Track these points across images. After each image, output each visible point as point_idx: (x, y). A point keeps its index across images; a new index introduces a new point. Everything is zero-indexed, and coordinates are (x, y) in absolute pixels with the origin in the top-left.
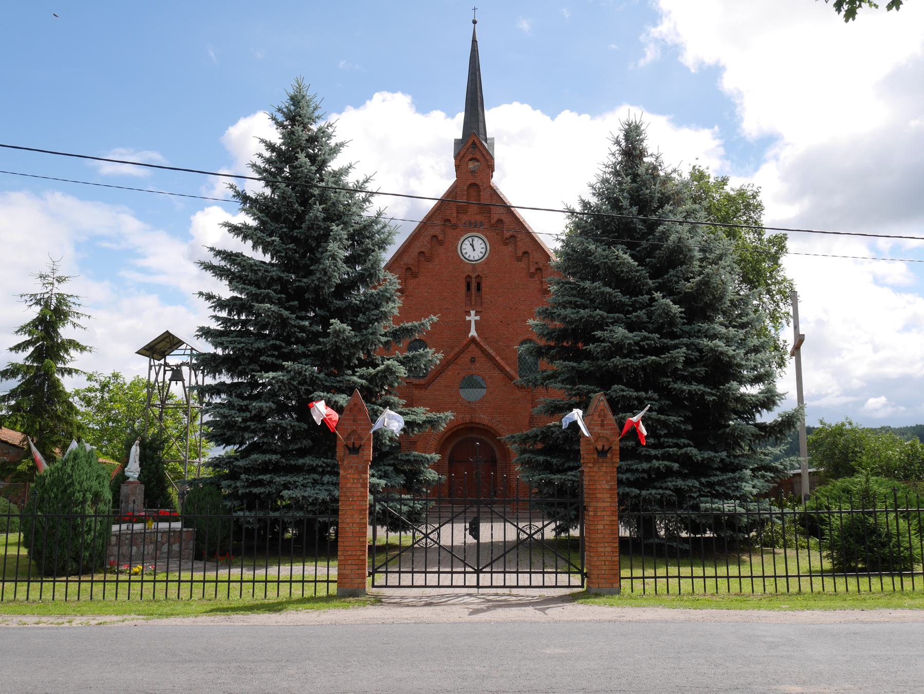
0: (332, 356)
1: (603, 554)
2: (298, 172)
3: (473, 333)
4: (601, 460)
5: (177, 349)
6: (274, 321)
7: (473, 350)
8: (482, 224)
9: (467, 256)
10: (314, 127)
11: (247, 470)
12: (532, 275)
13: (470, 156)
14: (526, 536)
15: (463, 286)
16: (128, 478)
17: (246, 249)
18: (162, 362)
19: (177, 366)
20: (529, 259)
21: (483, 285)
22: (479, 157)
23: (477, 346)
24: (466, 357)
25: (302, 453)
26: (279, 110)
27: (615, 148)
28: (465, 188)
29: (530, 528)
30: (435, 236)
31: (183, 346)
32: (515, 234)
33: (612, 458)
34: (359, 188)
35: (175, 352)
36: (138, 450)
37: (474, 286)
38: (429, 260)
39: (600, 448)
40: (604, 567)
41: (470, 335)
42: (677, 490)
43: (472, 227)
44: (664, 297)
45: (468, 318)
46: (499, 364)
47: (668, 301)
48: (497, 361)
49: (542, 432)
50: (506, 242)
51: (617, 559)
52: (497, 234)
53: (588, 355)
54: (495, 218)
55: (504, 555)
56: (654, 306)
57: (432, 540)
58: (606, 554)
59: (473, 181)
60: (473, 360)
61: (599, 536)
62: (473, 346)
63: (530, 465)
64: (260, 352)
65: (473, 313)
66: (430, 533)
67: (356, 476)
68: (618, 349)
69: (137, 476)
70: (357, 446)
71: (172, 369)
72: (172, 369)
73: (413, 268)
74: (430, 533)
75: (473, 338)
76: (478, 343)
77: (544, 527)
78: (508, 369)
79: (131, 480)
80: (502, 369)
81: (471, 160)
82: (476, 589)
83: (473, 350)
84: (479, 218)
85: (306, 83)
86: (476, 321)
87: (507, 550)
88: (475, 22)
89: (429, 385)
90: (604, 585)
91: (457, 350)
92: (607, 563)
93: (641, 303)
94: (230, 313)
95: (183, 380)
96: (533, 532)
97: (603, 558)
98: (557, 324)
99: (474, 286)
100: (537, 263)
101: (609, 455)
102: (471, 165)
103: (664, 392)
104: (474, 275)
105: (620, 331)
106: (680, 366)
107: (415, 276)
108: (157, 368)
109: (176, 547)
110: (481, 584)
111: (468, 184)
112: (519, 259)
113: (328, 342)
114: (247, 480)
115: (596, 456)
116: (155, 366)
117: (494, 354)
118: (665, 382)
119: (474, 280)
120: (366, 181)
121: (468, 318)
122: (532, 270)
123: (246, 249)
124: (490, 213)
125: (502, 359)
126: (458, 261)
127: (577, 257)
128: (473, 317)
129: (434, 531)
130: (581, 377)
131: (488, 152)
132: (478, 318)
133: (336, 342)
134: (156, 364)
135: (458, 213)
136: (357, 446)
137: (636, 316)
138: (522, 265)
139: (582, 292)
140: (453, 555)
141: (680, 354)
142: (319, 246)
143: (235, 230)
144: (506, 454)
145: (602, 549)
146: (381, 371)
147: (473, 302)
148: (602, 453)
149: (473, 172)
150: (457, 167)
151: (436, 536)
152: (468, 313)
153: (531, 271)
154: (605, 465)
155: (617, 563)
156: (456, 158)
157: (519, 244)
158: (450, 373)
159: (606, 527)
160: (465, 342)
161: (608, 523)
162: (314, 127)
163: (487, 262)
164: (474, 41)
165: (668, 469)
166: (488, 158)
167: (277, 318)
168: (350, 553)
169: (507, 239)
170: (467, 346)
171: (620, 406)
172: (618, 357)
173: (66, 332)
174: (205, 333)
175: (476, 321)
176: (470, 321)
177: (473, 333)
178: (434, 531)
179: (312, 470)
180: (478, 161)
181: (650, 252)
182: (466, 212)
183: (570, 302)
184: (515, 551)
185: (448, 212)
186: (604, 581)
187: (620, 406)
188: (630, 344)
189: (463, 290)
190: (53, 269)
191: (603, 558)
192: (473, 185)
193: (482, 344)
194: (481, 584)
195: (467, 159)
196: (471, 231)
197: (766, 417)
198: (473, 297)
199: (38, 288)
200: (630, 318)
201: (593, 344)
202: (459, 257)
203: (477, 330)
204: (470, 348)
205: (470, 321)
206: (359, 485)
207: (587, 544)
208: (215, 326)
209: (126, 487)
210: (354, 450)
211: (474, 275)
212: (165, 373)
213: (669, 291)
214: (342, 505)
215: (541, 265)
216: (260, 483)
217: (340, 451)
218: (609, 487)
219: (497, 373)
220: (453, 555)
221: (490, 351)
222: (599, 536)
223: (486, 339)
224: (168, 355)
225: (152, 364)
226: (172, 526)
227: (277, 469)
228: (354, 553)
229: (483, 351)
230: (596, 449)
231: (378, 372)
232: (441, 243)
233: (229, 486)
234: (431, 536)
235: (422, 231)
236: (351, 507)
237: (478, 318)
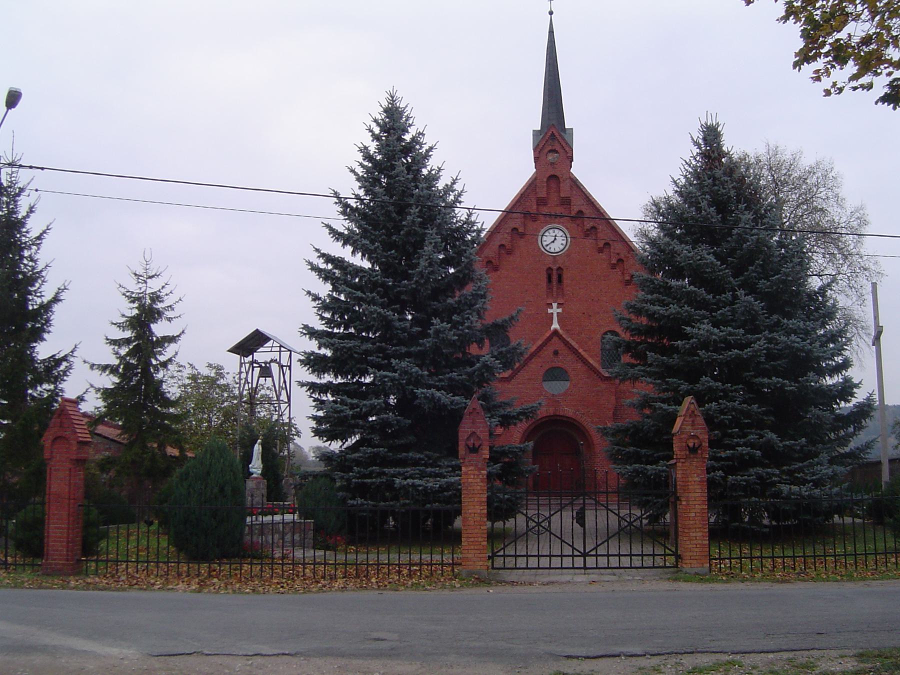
0: (431, 356)
1: (694, 539)
2: (395, 182)
3: (555, 326)
4: (692, 456)
5: (262, 346)
6: (379, 324)
7: (556, 344)
10: (407, 137)
11: (358, 463)
12: (613, 267)
13: (550, 148)
14: (626, 524)
15: (544, 276)
16: (252, 474)
17: (345, 253)
18: (250, 358)
19: (266, 363)
20: (610, 251)
21: (564, 276)
22: (558, 148)
23: (560, 339)
24: (548, 351)
25: (406, 448)
26: (376, 121)
27: (696, 150)
28: (545, 180)
29: (630, 517)
30: (515, 229)
31: (270, 344)
32: (596, 225)
33: (702, 454)
34: (449, 189)
35: (261, 349)
36: (261, 448)
37: (555, 277)
38: (510, 252)
39: (691, 445)
40: (696, 550)
41: (553, 327)
42: (760, 477)
43: (553, 218)
44: (745, 295)
45: (550, 311)
46: (582, 356)
47: (750, 298)
48: (580, 353)
49: (634, 426)
50: (588, 233)
51: (707, 542)
52: (578, 225)
53: (676, 350)
54: (575, 209)
55: (607, 541)
56: (737, 303)
57: (544, 528)
58: (698, 538)
59: (552, 173)
60: (556, 353)
61: (691, 522)
62: (555, 339)
63: (614, 458)
64: (367, 353)
65: (555, 305)
66: (542, 522)
67: (476, 472)
68: (705, 345)
69: (260, 472)
70: (477, 446)
71: (260, 366)
72: (260, 366)
73: (493, 261)
74: (542, 522)
75: (556, 332)
76: (561, 336)
77: (551, 515)
78: (591, 361)
79: (254, 475)
80: (585, 362)
81: (550, 151)
82: (583, 570)
83: (556, 344)
84: (559, 210)
85: (398, 95)
86: (558, 313)
87: (610, 535)
88: (551, 13)
89: (513, 378)
90: (696, 566)
91: (540, 342)
92: (698, 546)
93: (724, 301)
94: (333, 315)
95: (271, 376)
96: (632, 520)
97: (695, 542)
98: (644, 320)
99: (555, 277)
100: (618, 254)
101: (699, 452)
102: (551, 157)
103: (751, 387)
104: (555, 268)
105: (705, 328)
106: (763, 359)
107: (496, 269)
108: (247, 365)
109: (297, 537)
110: (587, 566)
111: (547, 176)
112: (600, 250)
113: (428, 342)
114: (359, 472)
115: (688, 453)
116: (245, 363)
117: (576, 346)
118: (747, 376)
119: (554, 272)
120: (454, 183)
121: (550, 311)
122: (614, 261)
123: (345, 253)
124: (570, 205)
125: (585, 351)
126: (540, 254)
127: (664, 259)
128: (555, 310)
129: (545, 520)
130: (670, 371)
131: (567, 144)
132: (560, 310)
133: (436, 342)
134: (246, 361)
135: (538, 205)
136: (477, 446)
137: (722, 314)
138: (603, 256)
139: (667, 290)
140: (562, 541)
141: (760, 344)
142: (415, 252)
143: (336, 235)
144: (590, 444)
145: (694, 534)
146: (479, 369)
147: (555, 294)
148: (693, 450)
149: (552, 164)
150: (536, 159)
151: (529, 524)
152: (550, 306)
153: (612, 262)
154: (696, 460)
155: (708, 546)
156: (535, 150)
158: (533, 366)
159: (698, 514)
160: (548, 335)
161: (699, 511)
162: (407, 137)
163: (568, 254)
164: (551, 32)
165: (752, 457)
167: (382, 321)
168: (472, 539)
169: (587, 230)
170: (549, 339)
171: (706, 398)
172: (704, 351)
173: (159, 329)
174: (311, 333)
175: (558, 313)
176: (552, 314)
177: (555, 326)
178: (545, 520)
179: (416, 463)
180: (557, 152)
181: (732, 252)
182: (545, 204)
183: (658, 300)
184: (617, 537)
185: (528, 204)
186: (695, 562)
187: (706, 398)
188: (715, 340)
189: (544, 284)
190: (146, 269)
191: (695, 542)
192: (553, 177)
193: (564, 336)
194: (587, 566)
195: (546, 151)
196: (551, 223)
197: (845, 407)
198: (555, 289)
199: (134, 287)
200: (715, 317)
201: (682, 341)
202: (540, 249)
203: (559, 322)
204: (553, 340)
205: (552, 314)
206: (479, 480)
207: (680, 529)
208: (320, 326)
209: (250, 482)
210: (474, 450)
211: (555, 268)
212: (253, 370)
213: (752, 289)
214: (465, 497)
215: (622, 256)
216: (370, 476)
217: (462, 451)
218: (699, 480)
219: (579, 365)
220: (562, 541)
221: (573, 343)
222: (691, 522)
223: (567, 331)
224: (256, 352)
225: (243, 361)
226: (285, 518)
227: (385, 462)
228: (476, 539)
229: (566, 343)
230: (688, 446)
231: (475, 371)
232: (522, 235)
233: (342, 478)
234: (543, 524)
235: (502, 223)
236: (473, 499)
237: (560, 310)
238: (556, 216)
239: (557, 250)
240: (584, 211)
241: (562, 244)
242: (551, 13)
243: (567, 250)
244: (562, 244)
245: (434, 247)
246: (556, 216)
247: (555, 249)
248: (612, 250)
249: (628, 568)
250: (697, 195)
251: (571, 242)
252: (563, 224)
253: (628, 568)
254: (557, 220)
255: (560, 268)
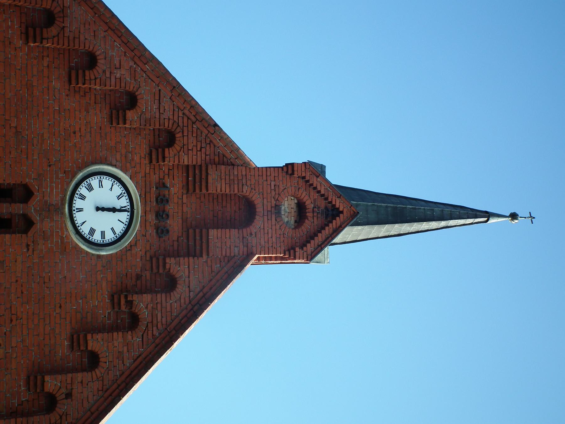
8: (161, 231)
9: (83, 190)
13: (310, 205)
22: (309, 225)
28: (246, 191)
59: (259, 209)
73: (53, 30)
81: (301, 207)
88: (514, 216)
100: (69, 395)
119: (18, 208)
157: (118, 337)
166: (310, 247)
182: (187, 188)
195: (304, 195)
202: (80, 169)
238: (161, 215)
239: (79, 218)
240: (175, 295)
241: (92, 231)
242: (514, 216)
243: (77, 247)
244: (92, 231)
245: (28, 267)
246: (161, 215)
247: (80, 210)
248: (79, 376)
249: (178, 115)
250: (115, 342)
251: (99, 256)
252: (143, 234)
253: (178, 115)
254: (151, 217)
255: (29, 223)
